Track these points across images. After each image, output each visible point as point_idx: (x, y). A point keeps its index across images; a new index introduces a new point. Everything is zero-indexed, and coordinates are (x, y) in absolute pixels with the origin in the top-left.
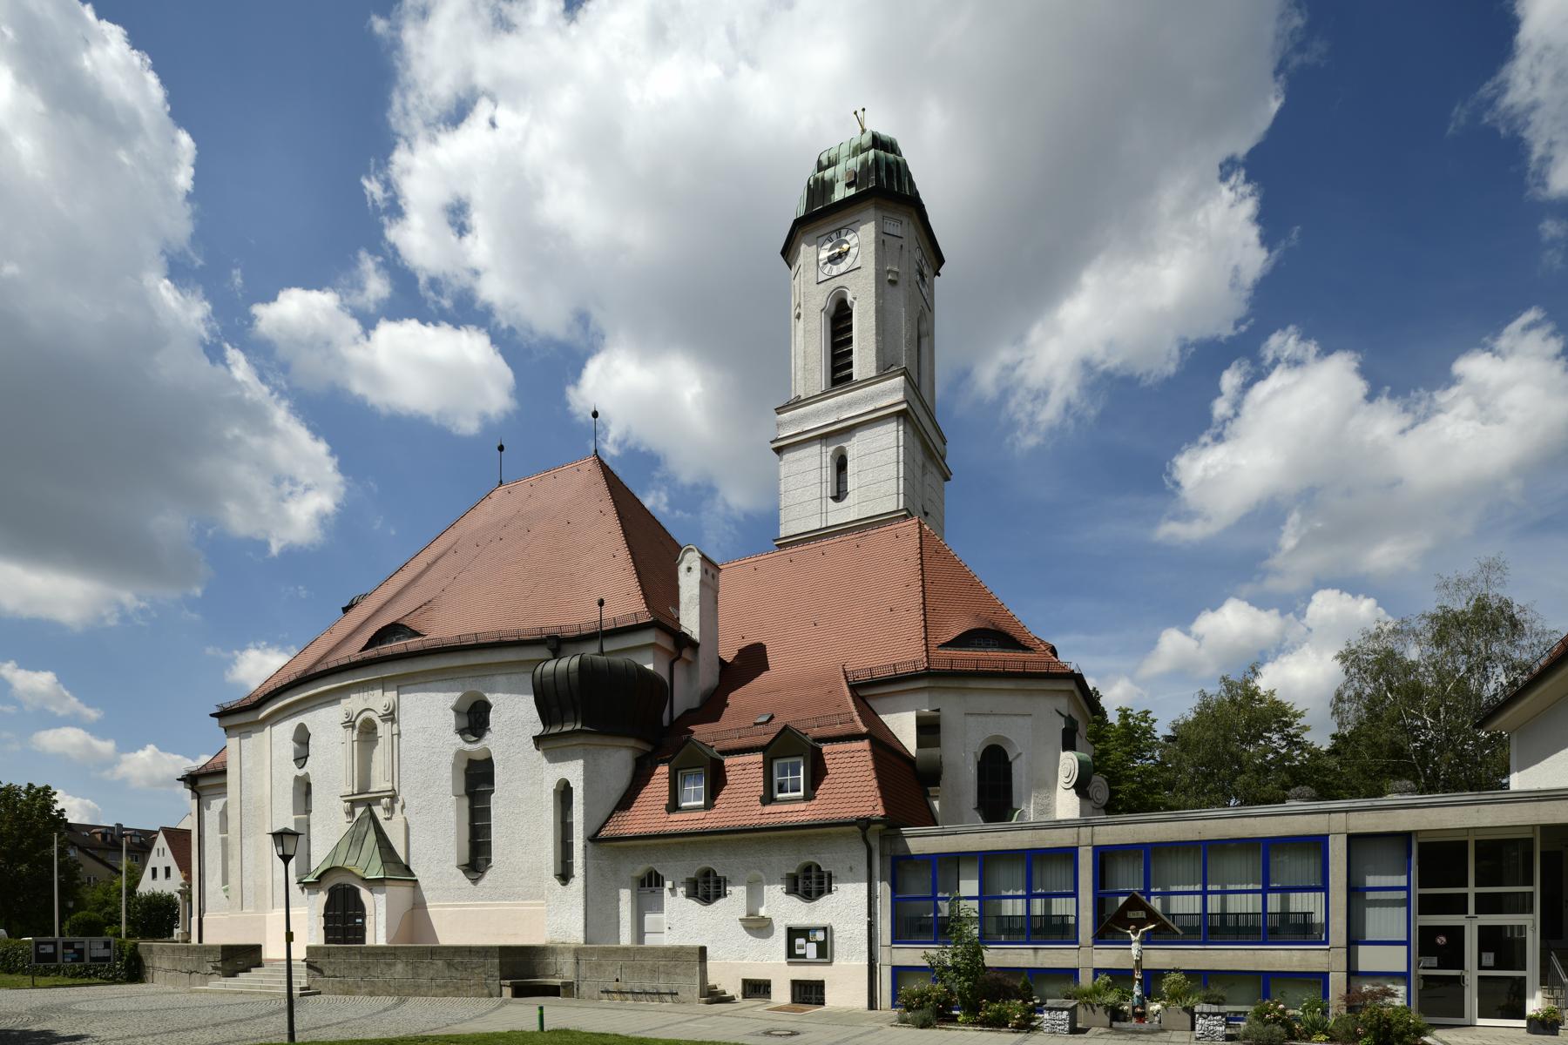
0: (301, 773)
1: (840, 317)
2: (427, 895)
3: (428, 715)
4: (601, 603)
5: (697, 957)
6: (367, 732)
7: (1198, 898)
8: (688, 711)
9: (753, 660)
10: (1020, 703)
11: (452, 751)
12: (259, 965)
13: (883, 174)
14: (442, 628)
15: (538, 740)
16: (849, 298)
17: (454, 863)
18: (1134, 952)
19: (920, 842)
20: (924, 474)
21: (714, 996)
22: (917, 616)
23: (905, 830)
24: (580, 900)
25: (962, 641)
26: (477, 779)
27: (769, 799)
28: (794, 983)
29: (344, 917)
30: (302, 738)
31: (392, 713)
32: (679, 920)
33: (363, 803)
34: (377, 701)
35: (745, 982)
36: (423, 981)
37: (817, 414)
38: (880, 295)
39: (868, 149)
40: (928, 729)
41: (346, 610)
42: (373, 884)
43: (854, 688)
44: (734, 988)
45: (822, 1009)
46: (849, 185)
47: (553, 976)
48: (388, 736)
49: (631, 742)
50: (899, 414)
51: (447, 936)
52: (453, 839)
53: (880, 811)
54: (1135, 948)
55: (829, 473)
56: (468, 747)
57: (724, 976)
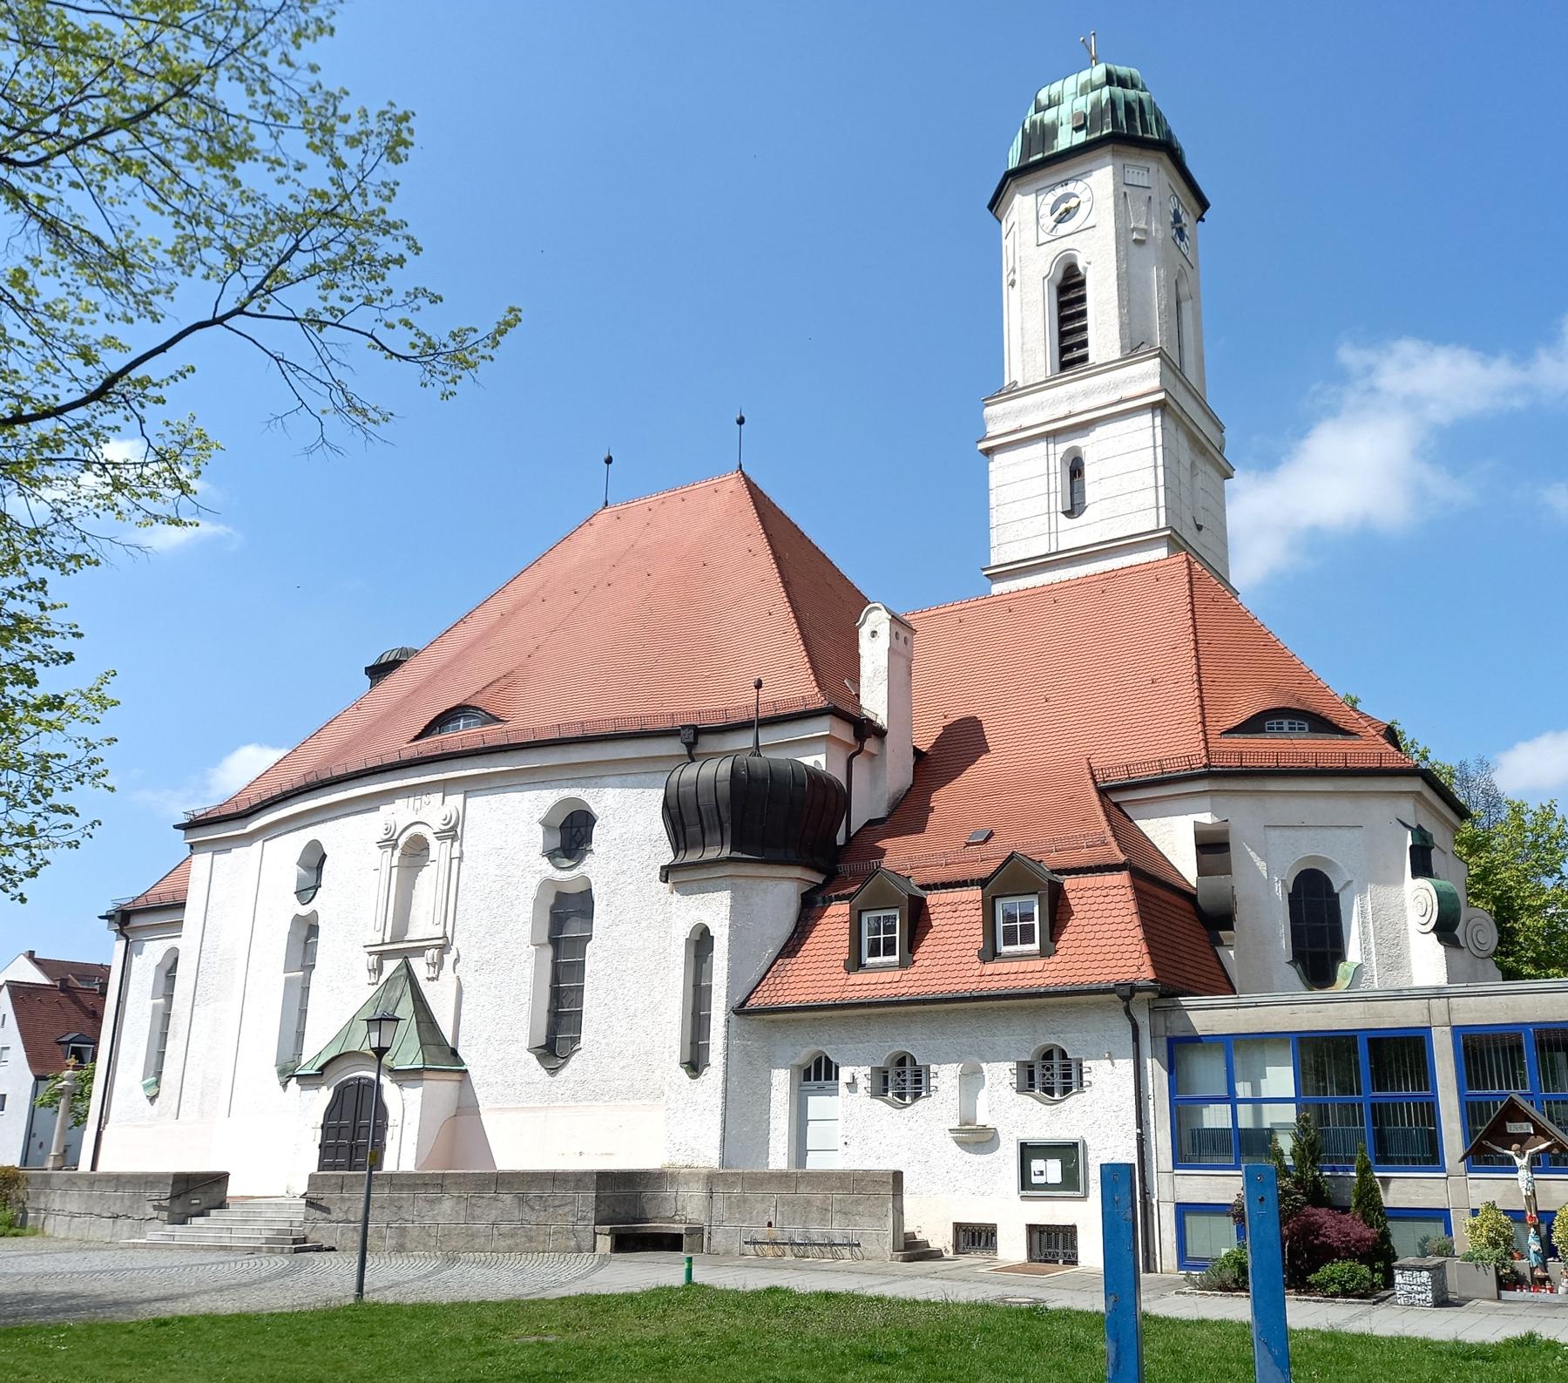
0: (304, 911)
1: (1069, 289)
2: (480, 1094)
3: (505, 827)
4: (759, 685)
5: (888, 1190)
6: (415, 852)
7: (1240, 1107)
8: (871, 823)
9: (961, 744)
10: (1342, 809)
11: (534, 883)
12: (222, 1205)
13: (1121, 114)
14: (530, 715)
15: (667, 872)
16: (1081, 265)
17: (677, 1057)
18: (1522, 1184)
19: (1207, 1016)
20: (1193, 476)
21: (914, 1250)
22: (1191, 691)
23: (1185, 1001)
24: (718, 1100)
25: (1254, 725)
26: (567, 920)
27: (990, 953)
28: (1032, 1229)
29: (352, 1131)
30: (314, 861)
31: (454, 828)
32: (853, 1128)
33: (399, 957)
34: (433, 811)
35: (959, 1227)
36: (480, 1226)
37: (1040, 406)
38: (1123, 257)
39: (1101, 86)
40: (1211, 846)
41: (378, 672)
42: (404, 1076)
43: (1103, 792)
44: (940, 1237)
45: (1072, 1270)
46: (1077, 129)
47: (672, 1220)
48: (444, 861)
49: (797, 872)
50: (1154, 407)
51: (510, 1155)
52: (527, 1008)
53: (1148, 973)
54: (1523, 1175)
55: (1059, 481)
56: (560, 875)
57: (931, 1220)
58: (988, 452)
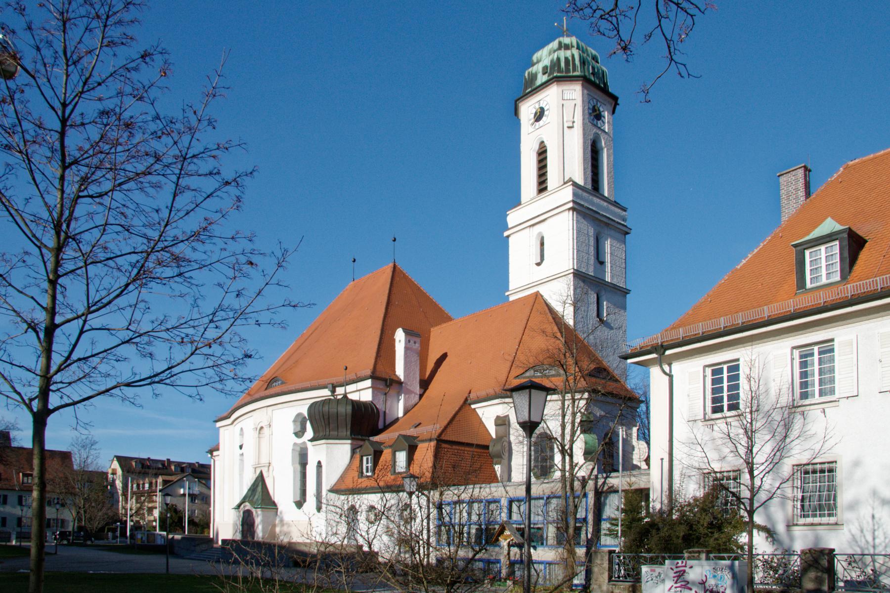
1: (542, 154)
13: (563, 65)
39: (555, 51)
58: (508, 237)
